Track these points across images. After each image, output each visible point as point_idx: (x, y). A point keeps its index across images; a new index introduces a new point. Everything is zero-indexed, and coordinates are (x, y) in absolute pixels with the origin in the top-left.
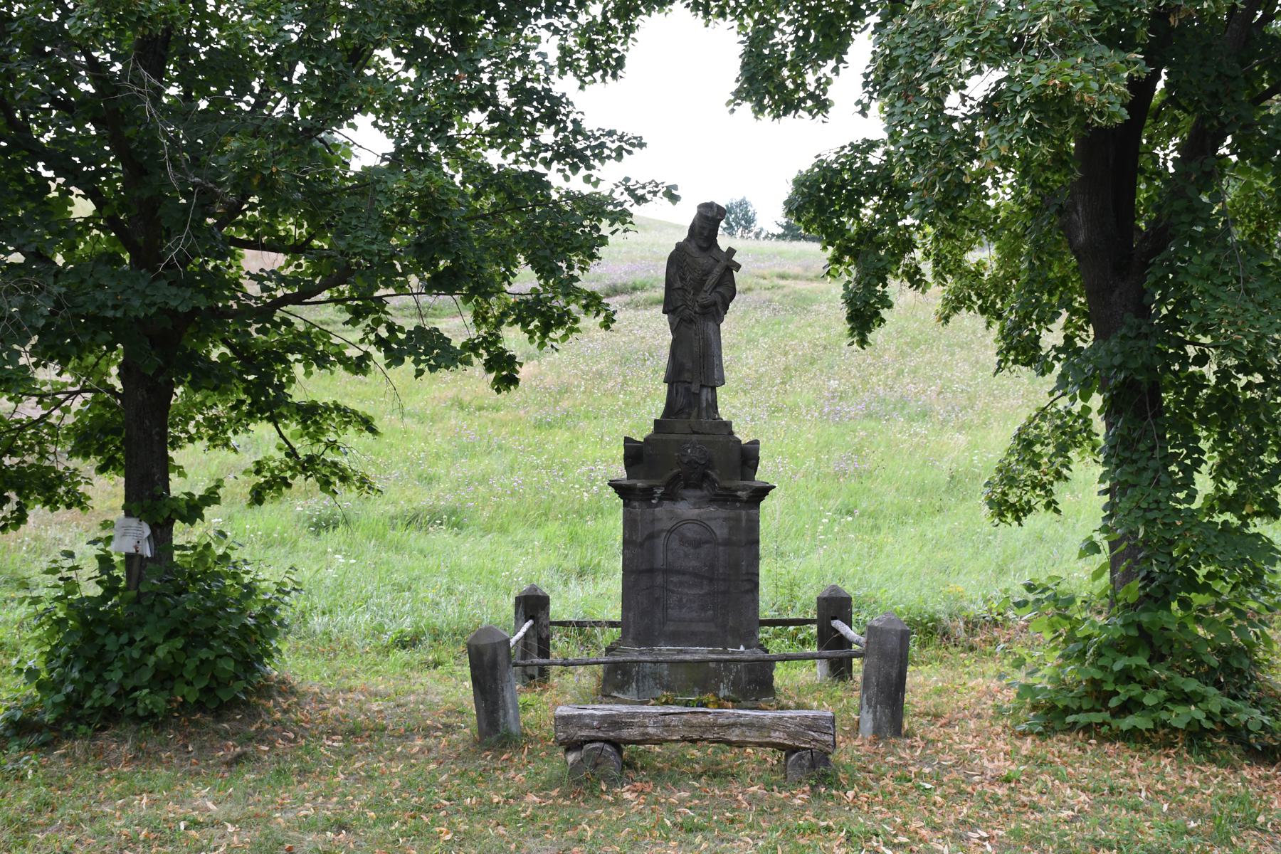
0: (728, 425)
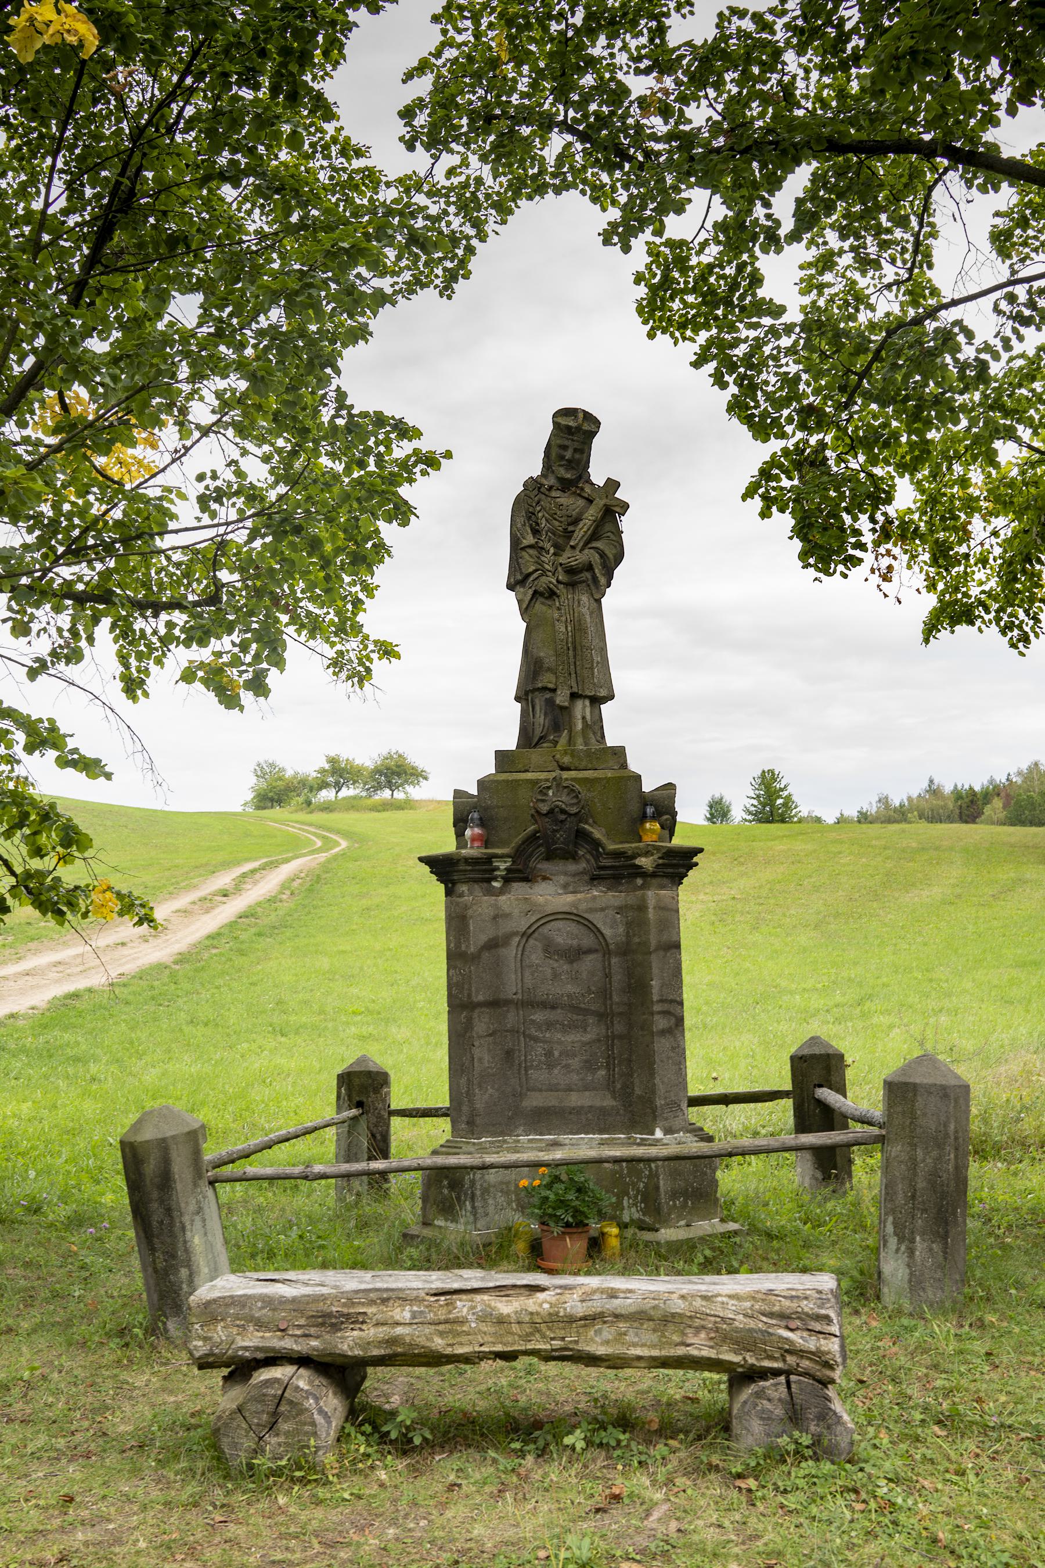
0: (619, 753)
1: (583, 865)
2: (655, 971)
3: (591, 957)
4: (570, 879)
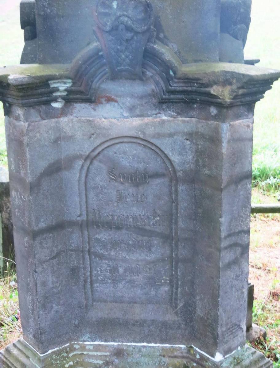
1: (151, 87)
2: (225, 207)
3: (158, 181)
4: (137, 102)
